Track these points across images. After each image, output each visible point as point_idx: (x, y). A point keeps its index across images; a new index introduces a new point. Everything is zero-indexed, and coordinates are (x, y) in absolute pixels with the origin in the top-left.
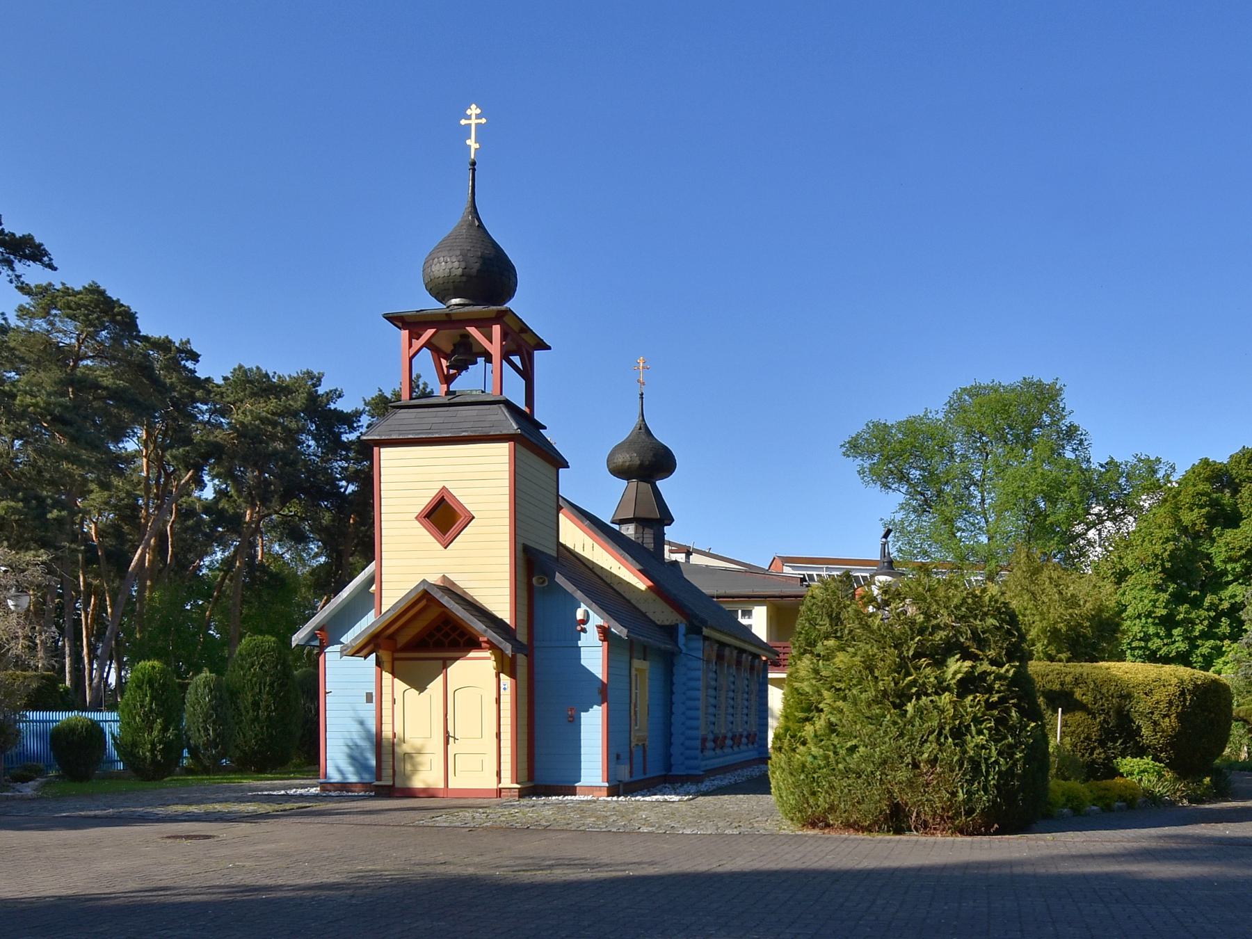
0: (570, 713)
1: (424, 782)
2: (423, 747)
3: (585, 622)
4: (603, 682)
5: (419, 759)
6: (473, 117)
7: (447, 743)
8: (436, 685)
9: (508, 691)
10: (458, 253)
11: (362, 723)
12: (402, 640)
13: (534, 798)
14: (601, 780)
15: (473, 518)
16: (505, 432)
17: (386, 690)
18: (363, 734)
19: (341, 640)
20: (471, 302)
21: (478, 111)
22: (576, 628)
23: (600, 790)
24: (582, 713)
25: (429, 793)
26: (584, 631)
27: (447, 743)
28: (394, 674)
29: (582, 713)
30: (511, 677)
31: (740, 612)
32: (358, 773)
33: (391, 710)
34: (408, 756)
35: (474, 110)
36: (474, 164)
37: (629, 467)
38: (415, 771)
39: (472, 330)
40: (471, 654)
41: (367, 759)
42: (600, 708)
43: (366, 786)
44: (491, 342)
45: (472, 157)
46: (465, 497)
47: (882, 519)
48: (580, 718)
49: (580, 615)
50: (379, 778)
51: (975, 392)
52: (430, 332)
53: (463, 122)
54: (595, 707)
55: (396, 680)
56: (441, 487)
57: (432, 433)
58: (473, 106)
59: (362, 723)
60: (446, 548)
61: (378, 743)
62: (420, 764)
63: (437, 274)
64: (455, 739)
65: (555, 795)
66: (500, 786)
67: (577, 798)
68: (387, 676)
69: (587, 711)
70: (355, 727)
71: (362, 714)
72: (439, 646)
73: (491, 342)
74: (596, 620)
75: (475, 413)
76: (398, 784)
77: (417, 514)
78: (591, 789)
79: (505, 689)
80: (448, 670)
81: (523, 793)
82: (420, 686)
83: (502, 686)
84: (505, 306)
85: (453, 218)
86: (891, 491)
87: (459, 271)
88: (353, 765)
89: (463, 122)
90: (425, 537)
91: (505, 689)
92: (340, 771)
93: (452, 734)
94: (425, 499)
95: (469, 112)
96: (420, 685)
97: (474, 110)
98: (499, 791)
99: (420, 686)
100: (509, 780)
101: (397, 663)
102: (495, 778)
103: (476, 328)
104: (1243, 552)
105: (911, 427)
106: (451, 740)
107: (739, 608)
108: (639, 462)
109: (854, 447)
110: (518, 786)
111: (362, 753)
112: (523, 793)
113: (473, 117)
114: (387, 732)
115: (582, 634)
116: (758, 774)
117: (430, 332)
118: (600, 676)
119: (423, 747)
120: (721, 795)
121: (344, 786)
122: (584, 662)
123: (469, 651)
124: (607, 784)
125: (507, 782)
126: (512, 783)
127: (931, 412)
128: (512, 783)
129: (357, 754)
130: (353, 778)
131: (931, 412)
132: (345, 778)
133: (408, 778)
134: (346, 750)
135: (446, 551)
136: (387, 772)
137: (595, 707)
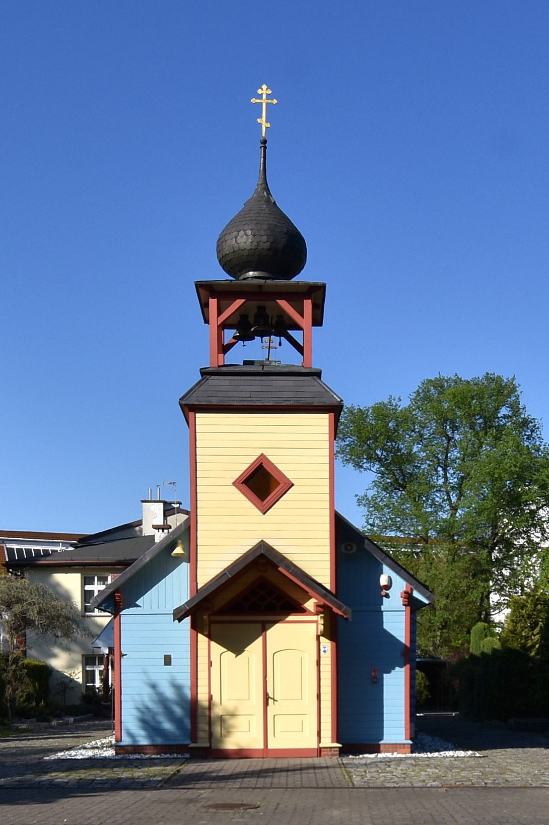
0: (373, 674)
1: (237, 744)
2: (236, 709)
3: (387, 587)
4: (405, 646)
5: (232, 721)
6: (264, 96)
7: (266, 704)
8: (254, 649)
9: (329, 653)
10: (266, 227)
11: (154, 686)
12: (219, 603)
13: (351, 756)
14: (404, 737)
15: (293, 485)
16: (328, 403)
18: (155, 697)
20: (270, 276)
21: (270, 92)
22: (379, 593)
23: (404, 748)
25: (241, 754)
26: (387, 596)
27: (266, 704)
28: (210, 637)
30: (208, 638)
31: (96, 578)
32: (150, 736)
33: (207, 673)
34: (221, 719)
35: (264, 90)
36: (265, 142)
39: (283, 304)
40: (290, 618)
41: (159, 723)
42: (403, 669)
43: (157, 748)
44: (303, 316)
45: (264, 135)
46: (283, 463)
47: (356, 496)
48: (382, 678)
49: (383, 581)
50: (194, 739)
51: (439, 384)
52: (239, 302)
53: (253, 100)
55: (212, 643)
56: (259, 454)
57: (278, 403)
58: (264, 87)
59: (154, 686)
60: (264, 514)
61: (193, 708)
62: (233, 727)
63: (242, 246)
64: (274, 700)
65: (361, 754)
66: (321, 745)
67: (380, 755)
68: (202, 639)
69: (389, 672)
70: (148, 690)
71: (155, 677)
72: (255, 609)
73: (303, 316)
74: (400, 585)
75: (291, 383)
77: (235, 479)
78: (395, 747)
80: (268, 632)
81: (343, 752)
82: (237, 649)
83: (322, 649)
85: (249, 189)
86: (362, 470)
87: (267, 245)
88: (144, 729)
89: (253, 100)
90: (242, 503)
91: (325, 651)
92: (131, 735)
93: (271, 695)
94: (242, 465)
95: (260, 91)
97: (264, 90)
98: (320, 751)
99: (237, 649)
100: (330, 740)
101: (213, 626)
102: (316, 738)
103: (287, 301)
105: (382, 412)
106: (270, 701)
107: (96, 575)
110: (340, 745)
111: (154, 718)
112: (343, 752)
113: (264, 96)
114: (203, 697)
115: (384, 598)
117: (239, 302)
118: (404, 642)
119: (236, 709)
120: (531, 747)
121: (136, 748)
122: (386, 626)
123: (288, 615)
124: (411, 742)
125: (327, 741)
126: (406, 739)
127: (394, 400)
129: (148, 717)
130: (144, 741)
131: (394, 400)
133: (220, 741)
134: (136, 713)
136: (202, 735)
137: (397, 668)
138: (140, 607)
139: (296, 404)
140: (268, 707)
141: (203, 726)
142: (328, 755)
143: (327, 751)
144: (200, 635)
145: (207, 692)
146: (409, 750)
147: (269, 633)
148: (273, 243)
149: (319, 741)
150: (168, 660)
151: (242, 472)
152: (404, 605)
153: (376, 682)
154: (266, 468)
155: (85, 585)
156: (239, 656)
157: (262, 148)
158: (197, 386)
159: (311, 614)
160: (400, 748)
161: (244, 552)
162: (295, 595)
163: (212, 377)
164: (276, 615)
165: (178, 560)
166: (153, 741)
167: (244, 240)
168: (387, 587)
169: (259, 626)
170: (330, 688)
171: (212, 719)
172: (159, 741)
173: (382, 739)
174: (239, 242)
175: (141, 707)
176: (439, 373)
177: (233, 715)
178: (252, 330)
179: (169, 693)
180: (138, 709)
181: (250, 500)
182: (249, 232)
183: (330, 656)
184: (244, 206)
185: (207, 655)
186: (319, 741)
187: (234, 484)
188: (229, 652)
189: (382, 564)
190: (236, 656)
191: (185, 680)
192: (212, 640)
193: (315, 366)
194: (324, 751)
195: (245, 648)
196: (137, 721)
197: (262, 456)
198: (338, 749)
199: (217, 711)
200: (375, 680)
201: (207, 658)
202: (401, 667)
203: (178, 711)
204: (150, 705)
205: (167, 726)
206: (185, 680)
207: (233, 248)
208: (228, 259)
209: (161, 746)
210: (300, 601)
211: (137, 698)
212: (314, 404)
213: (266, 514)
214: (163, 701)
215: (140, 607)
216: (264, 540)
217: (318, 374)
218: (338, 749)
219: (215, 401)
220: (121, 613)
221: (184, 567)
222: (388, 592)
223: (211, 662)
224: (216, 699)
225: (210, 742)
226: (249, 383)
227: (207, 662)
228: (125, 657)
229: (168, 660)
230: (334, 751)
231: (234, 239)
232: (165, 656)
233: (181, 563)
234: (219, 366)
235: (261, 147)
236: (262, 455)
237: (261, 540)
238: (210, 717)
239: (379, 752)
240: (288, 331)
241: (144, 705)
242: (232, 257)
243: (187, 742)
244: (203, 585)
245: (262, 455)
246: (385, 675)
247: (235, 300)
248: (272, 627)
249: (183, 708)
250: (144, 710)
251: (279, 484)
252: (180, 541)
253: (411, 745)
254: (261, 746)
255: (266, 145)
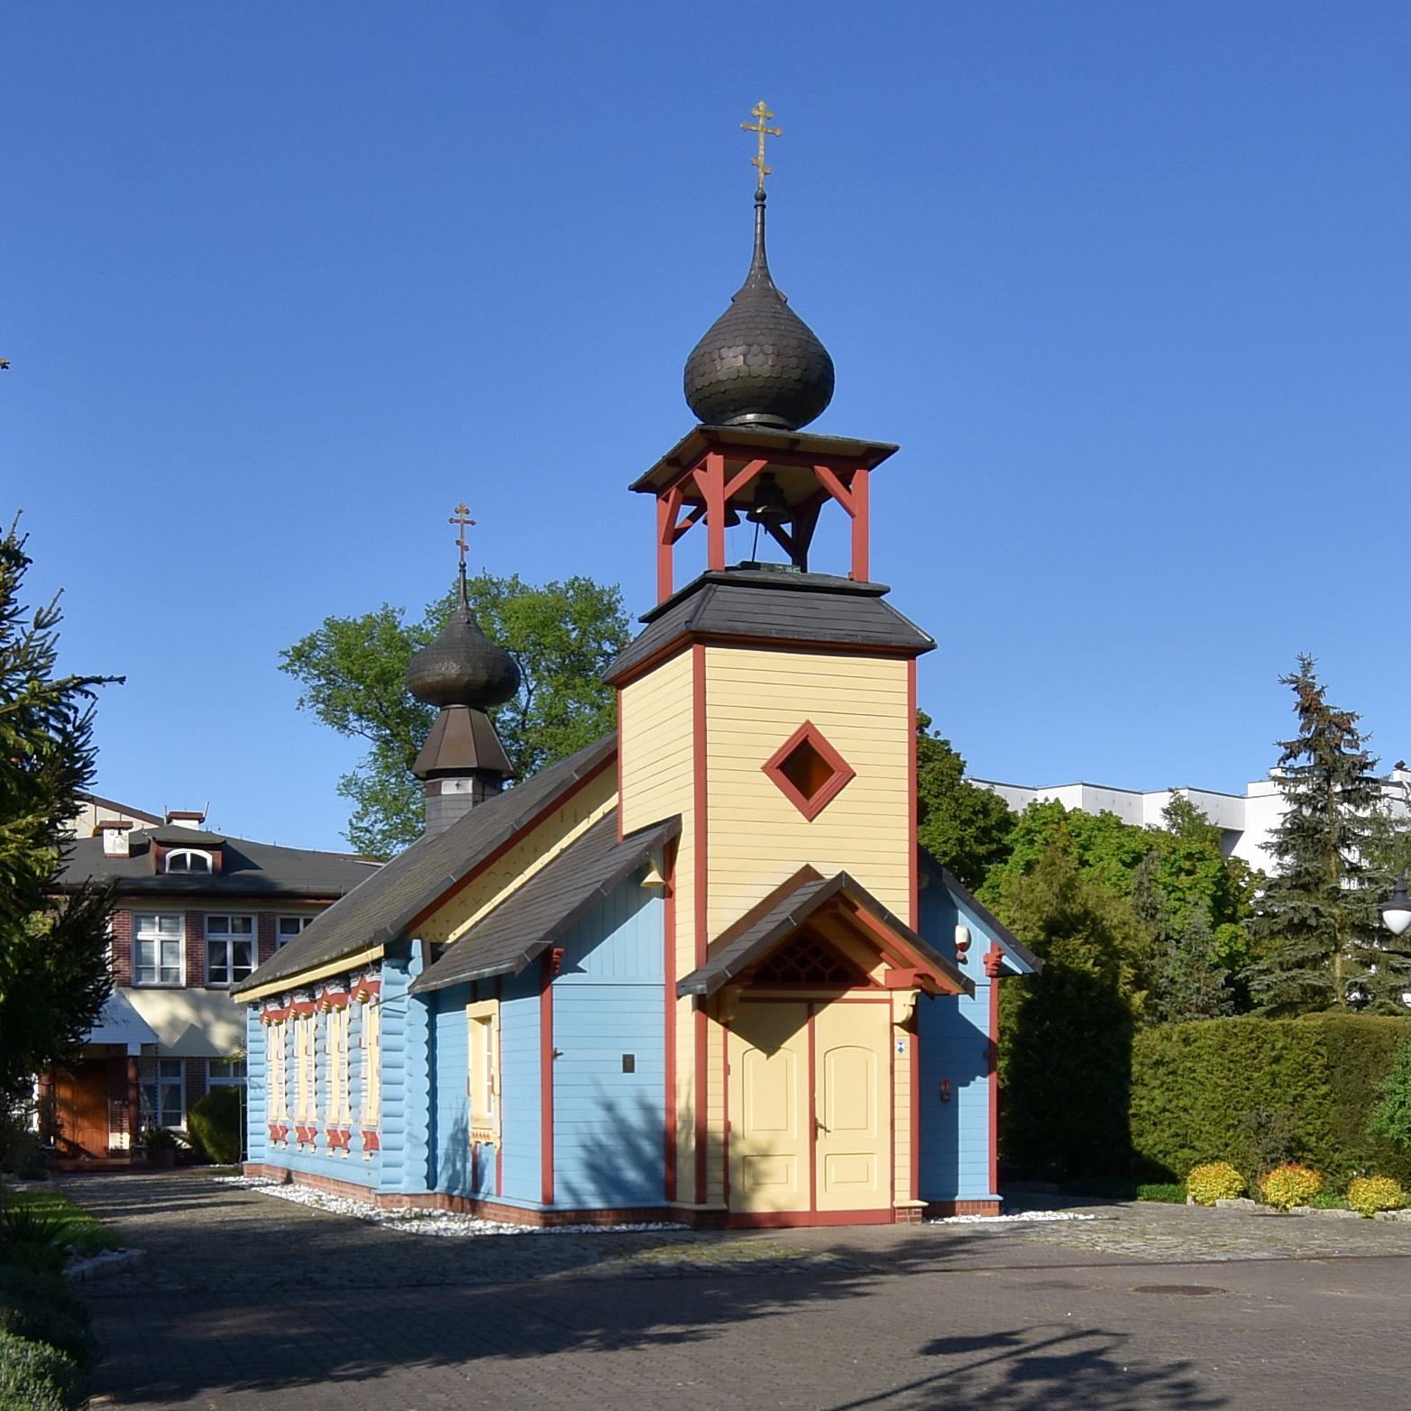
0: (943, 1087)
3: (965, 947)
4: (990, 1041)
5: (764, 1165)
7: (814, 1137)
8: (797, 1043)
9: (907, 1054)
10: (794, 343)
11: (609, 1107)
15: (854, 775)
17: (714, 1050)
18: (612, 1126)
19: (580, 965)
23: (989, 1207)
24: (960, 1089)
25: (781, 1221)
27: (814, 1137)
28: (727, 1026)
29: (960, 1089)
32: (603, 1194)
34: (746, 1161)
37: (468, 684)
38: (757, 1184)
40: (850, 994)
41: (618, 1170)
42: (987, 1080)
46: (841, 740)
49: (960, 936)
52: (756, 466)
54: (979, 1078)
55: (731, 1035)
59: (609, 1107)
60: (811, 821)
62: (765, 1174)
66: (896, 1205)
68: (714, 1027)
69: (967, 1084)
70: (600, 1115)
71: (611, 1092)
76: (733, 1209)
78: (976, 1206)
79: (901, 1050)
83: (897, 1046)
84: (798, 431)
85: (736, 277)
87: (796, 374)
88: (595, 1180)
90: (776, 800)
91: (901, 1050)
92: (572, 1191)
93: (821, 1122)
94: (776, 739)
96: (769, 1042)
98: (893, 1214)
99: (769, 1042)
103: (830, 469)
104: (947, 859)
106: (820, 1131)
108: (486, 678)
109: (301, 656)
110: (925, 1204)
111: (609, 1161)
114: (715, 1124)
116: (1177, 1171)
117: (756, 466)
118: (988, 1035)
123: (847, 988)
125: (905, 1198)
126: (912, 1199)
128: (912, 1199)
129: (600, 1161)
130: (595, 1203)
132: (579, 1202)
133: (746, 1197)
134: (581, 1153)
135: (811, 826)
136: (715, 1188)
138: (584, 971)
139: (865, 642)
140: (817, 1142)
141: (715, 1172)
142: (905, 1220)
143: (905, 1213)
144: (711, 1022)
145: (722, 1116)
146: (997, 1209)
147: (819, 1018)
148: (806, 370)
149: (893, 1198)
150: (629, 1064)
151: (777, 749)
152: (990, 976)
153: (948, 1100)
154: (814, 745)
155: (1052, 935)
156: (772, 1057)
157: (759, 208)
158: (704, 600)
159: (878, 987)
160: (984, 1207)
161: (780, 883)
162: (858, 956)
163: (721, 587)
164: (823, 988)
165: (645, 895)
166: (609, 1201)
167: (733, 361)
168: (965, 947)
169: (804, 1006)
170: (908, 1110)
171: (730, 1161)
172: (619, 1201)
173: (957, 1194)
174: (749, 362)
175: (589, 1143)
176: (473, 523)
177: (765, 1155)
178: (759, 511)
179: (635, 1119)
180: (584, 1147)
181: (789, 797)
182: (769, 349)
183: (908, 1057)
184: (731, 302)
185: (722, 1054)
186: (893, 1198)
187: (765, 769)
188: (757, 1050)
189: (955, 908)
190: (768, 1057)
191: (657, 1098)
192: (731, 1030)
193: (875, 579)
194: (899, 1214)
195: (783, 1043)
196: (582, 1168)
197: (808, 725)
198: (920, 1210)
199: (741, 1148)
200: (946, 1097)
201: (722, 1060)
202: (984, 1076)
203: (648, 1149)
204: (604, 1139)
205: (632, 1175)
206: (657, 1098)
207: (738, 372)
208: (723, 389)
209: (627, 1210)
210: (865, 967)
211: (584, 1128)
212: (893, 644)
213: (814, 821)
214: (623, 1131)
215: (584, 971)
216: (811, 864)
217: (877, 593)
218: (920, 1210)
219: (741, 628)
220: (554, 982)
221: (656, 904)
222: (965, 953)
223: (729, 1066)
224: (736, 1126)
225: (726, 1201)
226: (784, 601)
227: (722, 1066)
228: (559, 1057)
229: (629, 1064)
230: (916, 1213)
231: (742, 358)
232: (625, 1056)
233: (650, 899)
234: (728, 569)
235: (756, 207)
236: (808, 722)
237: (805, 864)
238: (726, 1157)
239: (953, 1214)
240: (695, 507)
241: (593, 1139)
242: (731, 387)
243: (663, 1203)
244: (716, 936)
245: (808, 722)
246: (961, 1090)
247: (750, 461)
248: (824, 1007)
249: (656, 1144)
250: (596, 1149)
251: (833, 772)
252: (653, 861)
253: (1000, 1202)
254: (806, 1207)
255: (765, 202)
